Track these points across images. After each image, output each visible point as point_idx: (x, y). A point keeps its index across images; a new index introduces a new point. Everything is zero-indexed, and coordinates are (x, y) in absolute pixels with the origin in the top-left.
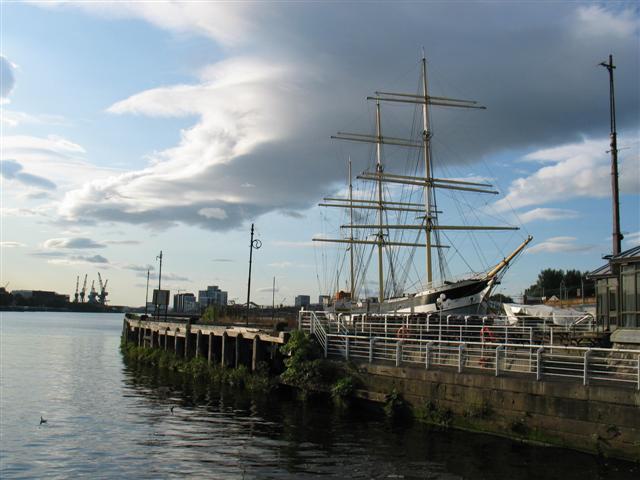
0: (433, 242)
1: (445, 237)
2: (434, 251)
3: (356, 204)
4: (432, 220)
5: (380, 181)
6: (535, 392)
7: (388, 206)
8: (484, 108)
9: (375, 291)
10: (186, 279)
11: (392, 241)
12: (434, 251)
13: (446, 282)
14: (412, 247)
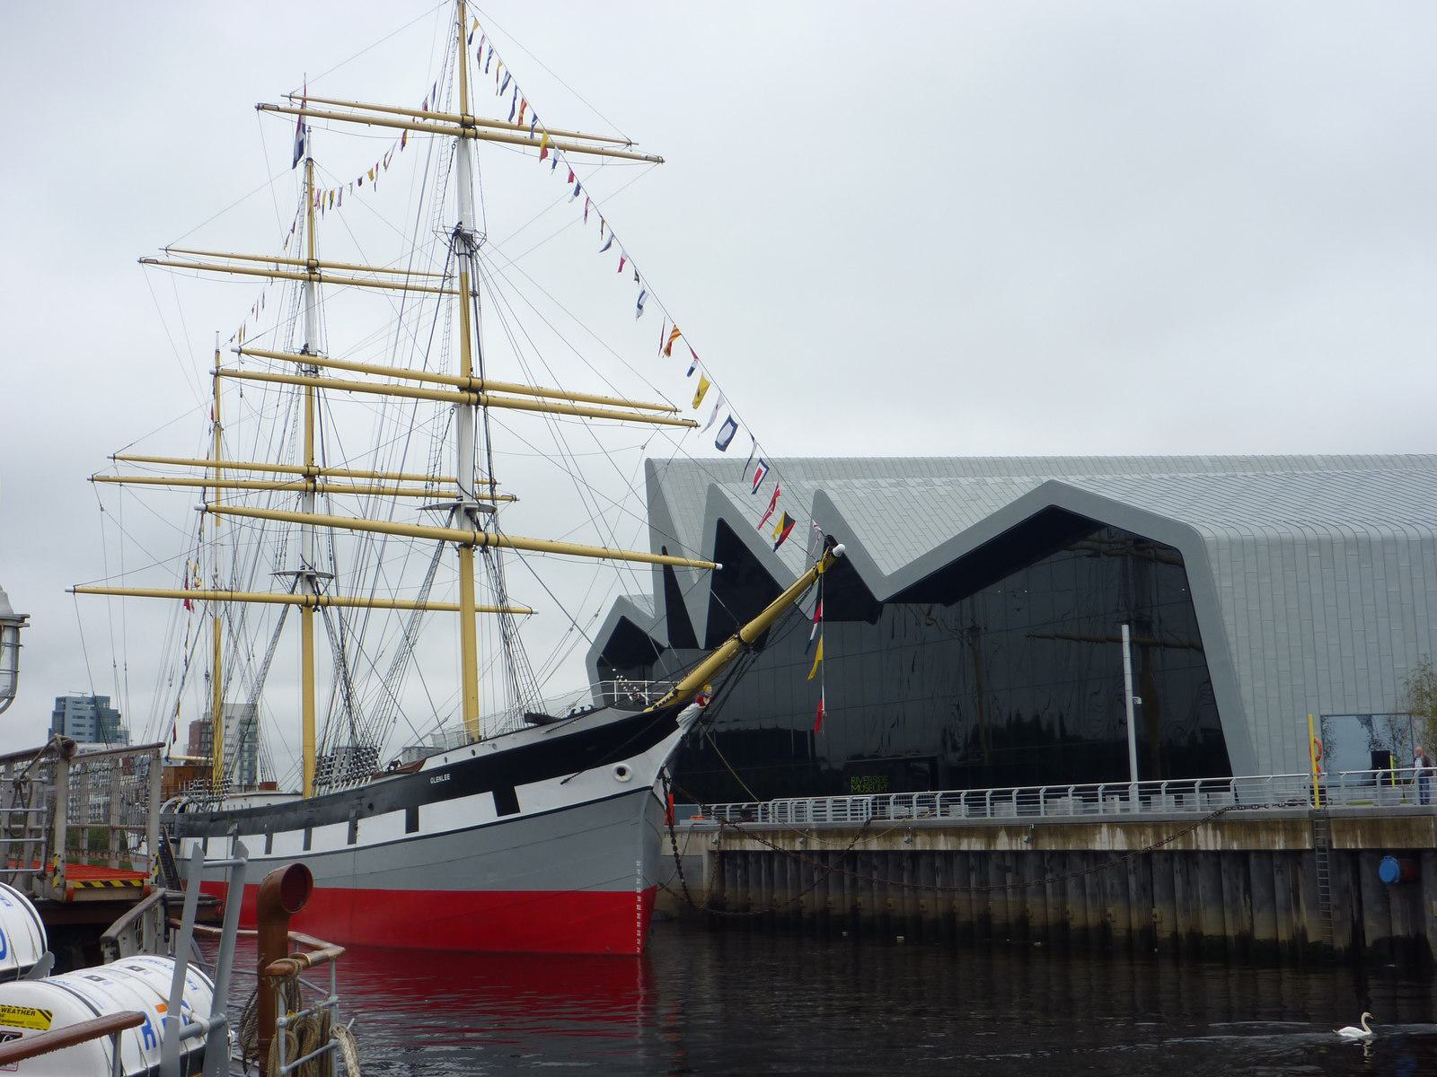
0: (483, 594)
1: (517, 571)
2: (487, 627)
3: (232, 475)
4: (482, 517)
5: (310, 385)
6: (477, 382)
7: (335, 481)
8: (659, 160)
9: (315, 614)
10: (480, 49)
11: (344, 595)
12: (487, 627)
13: (529, 717)
14: (407, 614)
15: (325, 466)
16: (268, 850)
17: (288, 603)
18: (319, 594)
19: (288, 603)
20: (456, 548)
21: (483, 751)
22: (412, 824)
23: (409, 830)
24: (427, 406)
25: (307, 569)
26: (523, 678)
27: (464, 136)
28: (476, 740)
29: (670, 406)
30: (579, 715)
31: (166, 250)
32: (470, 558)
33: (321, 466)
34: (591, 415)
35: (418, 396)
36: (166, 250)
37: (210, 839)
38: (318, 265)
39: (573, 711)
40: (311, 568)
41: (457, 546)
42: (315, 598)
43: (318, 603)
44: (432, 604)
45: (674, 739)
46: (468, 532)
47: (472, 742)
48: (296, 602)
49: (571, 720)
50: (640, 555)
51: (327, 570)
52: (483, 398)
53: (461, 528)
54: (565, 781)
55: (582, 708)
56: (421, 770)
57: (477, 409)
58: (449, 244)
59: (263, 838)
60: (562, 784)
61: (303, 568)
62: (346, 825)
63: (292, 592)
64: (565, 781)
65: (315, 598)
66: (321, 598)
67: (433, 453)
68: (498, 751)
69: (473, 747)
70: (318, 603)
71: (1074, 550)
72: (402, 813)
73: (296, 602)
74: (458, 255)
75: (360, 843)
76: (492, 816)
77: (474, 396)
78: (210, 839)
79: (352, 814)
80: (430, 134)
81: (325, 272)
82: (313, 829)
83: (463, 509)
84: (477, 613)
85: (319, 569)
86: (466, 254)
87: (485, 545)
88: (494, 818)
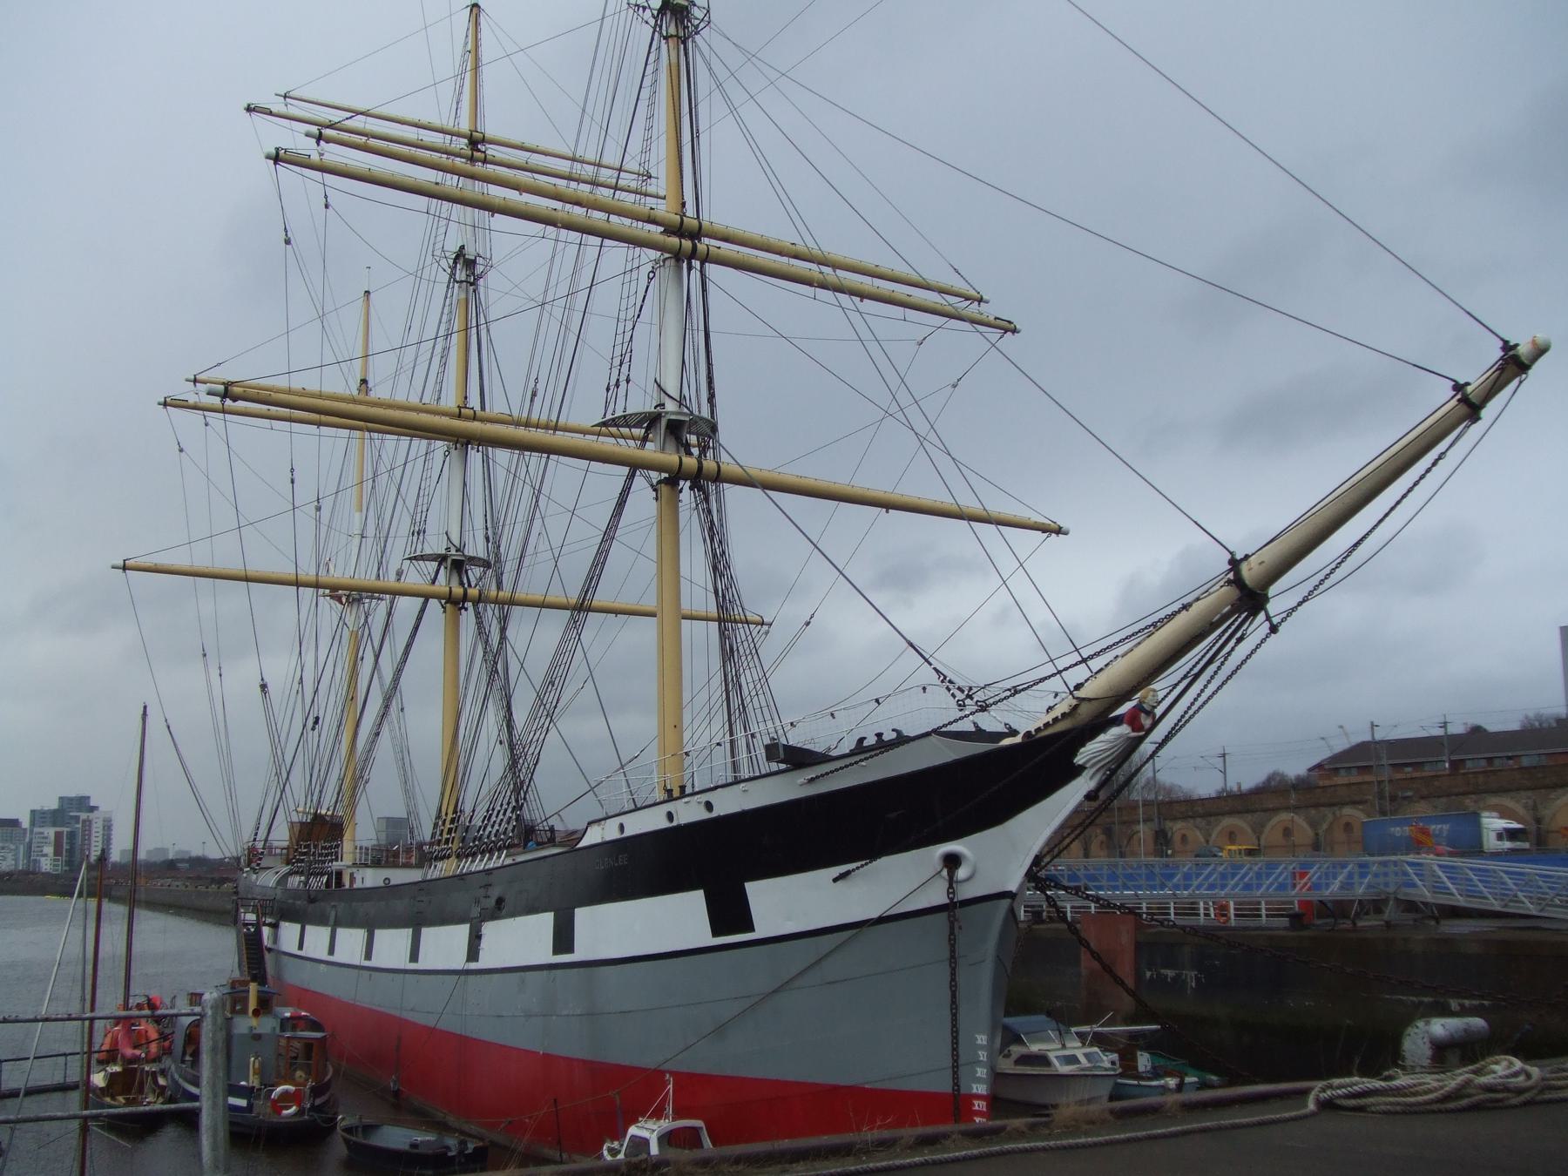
6: (691, 222)
17: (427, 597)
18: (470, 585)
21: (689, 812)
22: (564, 938)
23: (557, 951)
24: (617, 253)
25: (453, 552)
28: (676, 793)
29: (973, 293)
30: (871, 748)
31: (285, 97)
32: (675, 503)
33: (478, 408)
34: (863, 295)
36: (285, 97)
37: (308, 928)
38: (483, 141)
39: (861, 740)
41: (655, 482)
44: (584, 254)
45: (1071, 796)
46: (671, 458)
47: (670, 797)
48: (438, 597)
49: (857, 758)
50: (938, 505)
52: (701, 247)
53: (663, 450)
55: (879, 735)
56: (580, 845)
60: (835, 880)
61: (448, 549)
62: (463, 931)
63: (433, 582)
66: (470, 591)
67: (624, 302)
68: (714, 814)
70: (465, 598)
71: (979, 735)
72: (548, 918)
73: (438, 597)
74: (666, 38)
76: (705, 938)
77: (687, 244)
78: (308, 928)
79: (475, 912)
81: (492, 151)
82: (423, 929)
83: (664, 422)
85: (470, 551)
87: (698, 479)
88: (705, 938)
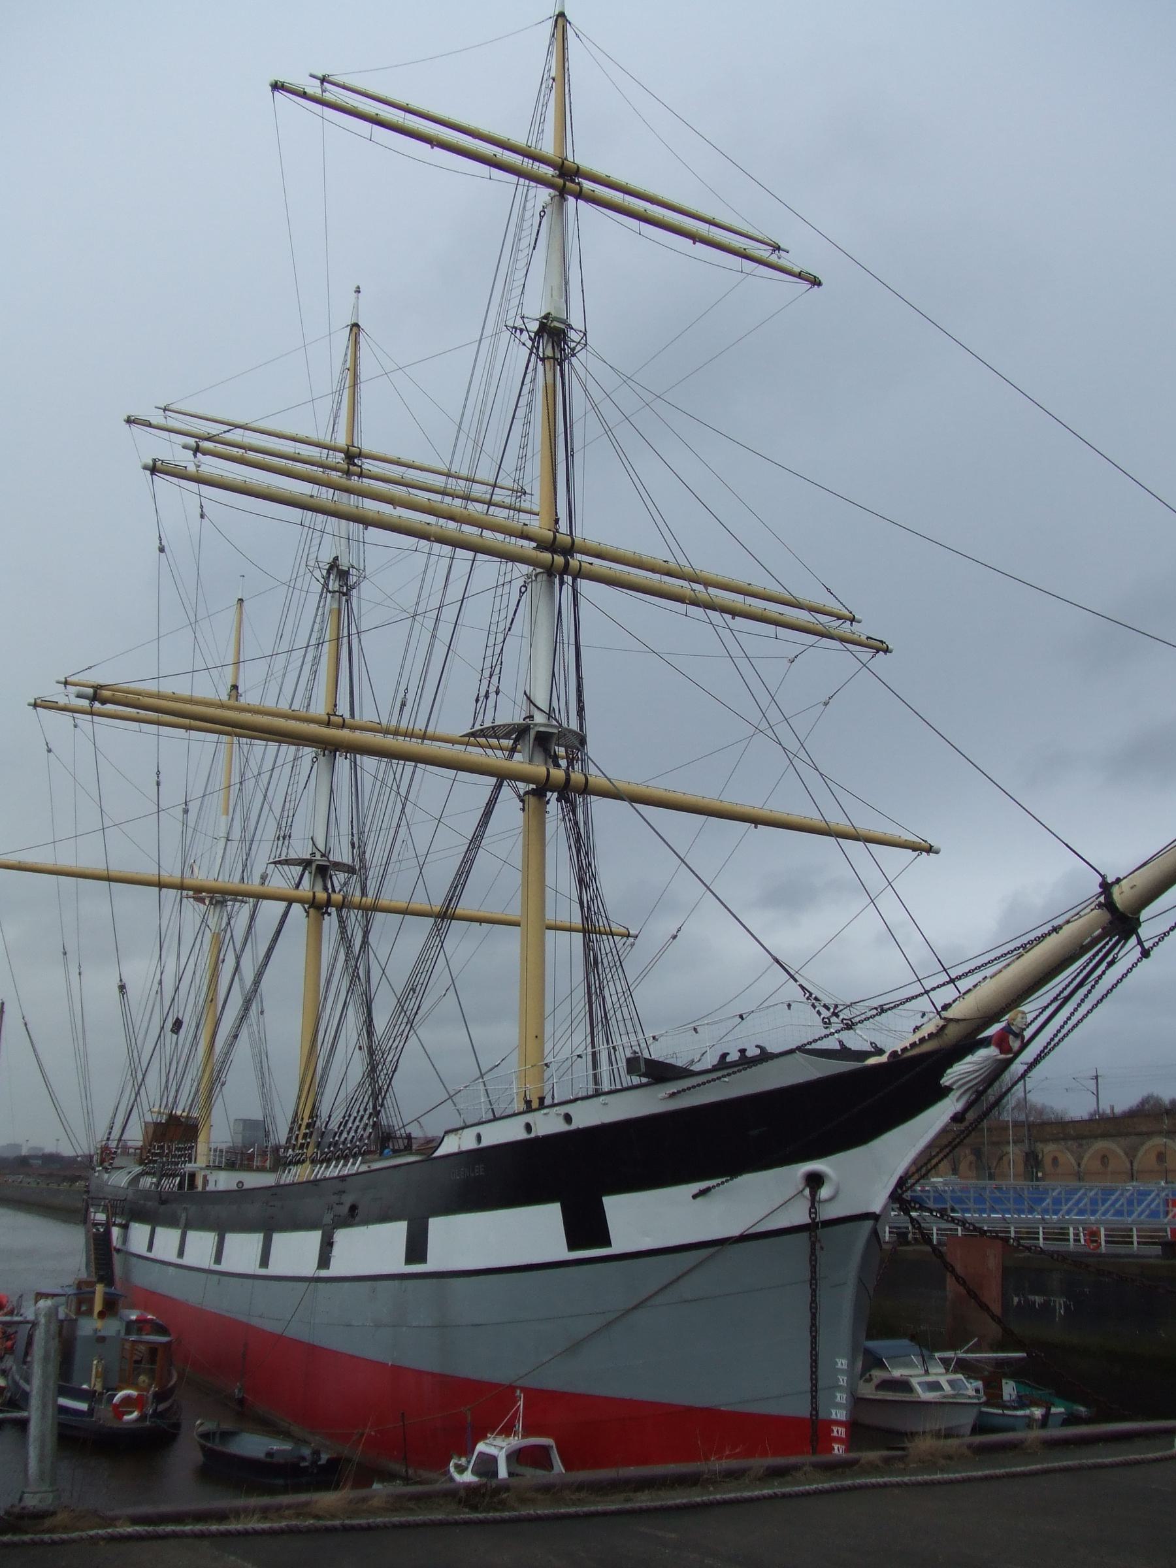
6: (563, 538)
15: (352, 715)
16: (265, 1261)
17: (290, 901)
18: (334, 891)
19: (290, 901)
20: (519, 796)
21: (547, 1124)
22: (416, 1249)
24: (489, 568)
25: (318, 857)
26: (621, 1024)
27: (562, 193)
30: (733, 1064)
32: (542, 813)
33: (347, 715)
34: (734, 613)
35: (476, 549)
38: (360, 455)
40: (323, 855)
42: (325, 896)
43: (329, 903)
48: (301, 901)
49: (719, 1074)
51: (346, 858)
52: (573, 563)
54: (703, 1193)
55: (743, 1051)
57: (562, 583)
58: (529, 344)
59: (257, 1238)
61: (313, 854)
63: (297, 886)
64: (703, 1193)
65: (325, 896)
68: (573, 1127)
69: (528, 1118)
70: (329, 903)
73: (301, 901)
74: (543, 360)
75: (336, 1269)
77: (559, 560)
79: (328, 1218)
80: (514, 178)
83: (532, 734)
84: (550, 934)
85: (335, 857)
86: (554, 358)
87: (565, 791)
